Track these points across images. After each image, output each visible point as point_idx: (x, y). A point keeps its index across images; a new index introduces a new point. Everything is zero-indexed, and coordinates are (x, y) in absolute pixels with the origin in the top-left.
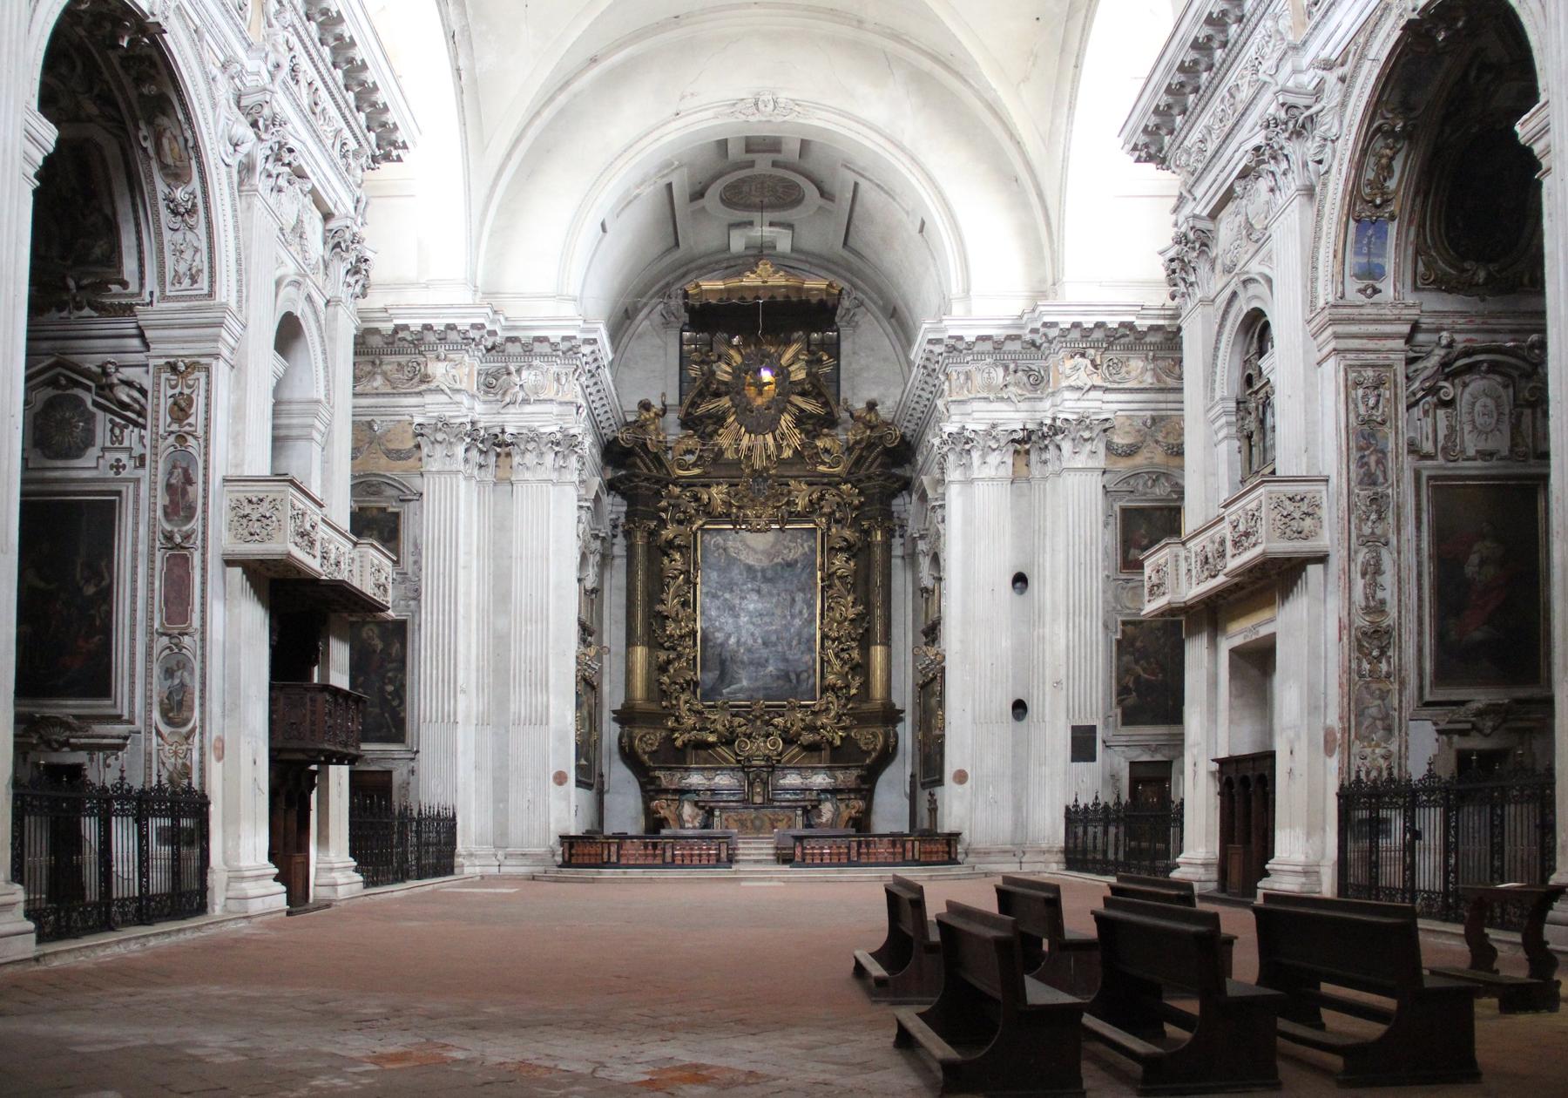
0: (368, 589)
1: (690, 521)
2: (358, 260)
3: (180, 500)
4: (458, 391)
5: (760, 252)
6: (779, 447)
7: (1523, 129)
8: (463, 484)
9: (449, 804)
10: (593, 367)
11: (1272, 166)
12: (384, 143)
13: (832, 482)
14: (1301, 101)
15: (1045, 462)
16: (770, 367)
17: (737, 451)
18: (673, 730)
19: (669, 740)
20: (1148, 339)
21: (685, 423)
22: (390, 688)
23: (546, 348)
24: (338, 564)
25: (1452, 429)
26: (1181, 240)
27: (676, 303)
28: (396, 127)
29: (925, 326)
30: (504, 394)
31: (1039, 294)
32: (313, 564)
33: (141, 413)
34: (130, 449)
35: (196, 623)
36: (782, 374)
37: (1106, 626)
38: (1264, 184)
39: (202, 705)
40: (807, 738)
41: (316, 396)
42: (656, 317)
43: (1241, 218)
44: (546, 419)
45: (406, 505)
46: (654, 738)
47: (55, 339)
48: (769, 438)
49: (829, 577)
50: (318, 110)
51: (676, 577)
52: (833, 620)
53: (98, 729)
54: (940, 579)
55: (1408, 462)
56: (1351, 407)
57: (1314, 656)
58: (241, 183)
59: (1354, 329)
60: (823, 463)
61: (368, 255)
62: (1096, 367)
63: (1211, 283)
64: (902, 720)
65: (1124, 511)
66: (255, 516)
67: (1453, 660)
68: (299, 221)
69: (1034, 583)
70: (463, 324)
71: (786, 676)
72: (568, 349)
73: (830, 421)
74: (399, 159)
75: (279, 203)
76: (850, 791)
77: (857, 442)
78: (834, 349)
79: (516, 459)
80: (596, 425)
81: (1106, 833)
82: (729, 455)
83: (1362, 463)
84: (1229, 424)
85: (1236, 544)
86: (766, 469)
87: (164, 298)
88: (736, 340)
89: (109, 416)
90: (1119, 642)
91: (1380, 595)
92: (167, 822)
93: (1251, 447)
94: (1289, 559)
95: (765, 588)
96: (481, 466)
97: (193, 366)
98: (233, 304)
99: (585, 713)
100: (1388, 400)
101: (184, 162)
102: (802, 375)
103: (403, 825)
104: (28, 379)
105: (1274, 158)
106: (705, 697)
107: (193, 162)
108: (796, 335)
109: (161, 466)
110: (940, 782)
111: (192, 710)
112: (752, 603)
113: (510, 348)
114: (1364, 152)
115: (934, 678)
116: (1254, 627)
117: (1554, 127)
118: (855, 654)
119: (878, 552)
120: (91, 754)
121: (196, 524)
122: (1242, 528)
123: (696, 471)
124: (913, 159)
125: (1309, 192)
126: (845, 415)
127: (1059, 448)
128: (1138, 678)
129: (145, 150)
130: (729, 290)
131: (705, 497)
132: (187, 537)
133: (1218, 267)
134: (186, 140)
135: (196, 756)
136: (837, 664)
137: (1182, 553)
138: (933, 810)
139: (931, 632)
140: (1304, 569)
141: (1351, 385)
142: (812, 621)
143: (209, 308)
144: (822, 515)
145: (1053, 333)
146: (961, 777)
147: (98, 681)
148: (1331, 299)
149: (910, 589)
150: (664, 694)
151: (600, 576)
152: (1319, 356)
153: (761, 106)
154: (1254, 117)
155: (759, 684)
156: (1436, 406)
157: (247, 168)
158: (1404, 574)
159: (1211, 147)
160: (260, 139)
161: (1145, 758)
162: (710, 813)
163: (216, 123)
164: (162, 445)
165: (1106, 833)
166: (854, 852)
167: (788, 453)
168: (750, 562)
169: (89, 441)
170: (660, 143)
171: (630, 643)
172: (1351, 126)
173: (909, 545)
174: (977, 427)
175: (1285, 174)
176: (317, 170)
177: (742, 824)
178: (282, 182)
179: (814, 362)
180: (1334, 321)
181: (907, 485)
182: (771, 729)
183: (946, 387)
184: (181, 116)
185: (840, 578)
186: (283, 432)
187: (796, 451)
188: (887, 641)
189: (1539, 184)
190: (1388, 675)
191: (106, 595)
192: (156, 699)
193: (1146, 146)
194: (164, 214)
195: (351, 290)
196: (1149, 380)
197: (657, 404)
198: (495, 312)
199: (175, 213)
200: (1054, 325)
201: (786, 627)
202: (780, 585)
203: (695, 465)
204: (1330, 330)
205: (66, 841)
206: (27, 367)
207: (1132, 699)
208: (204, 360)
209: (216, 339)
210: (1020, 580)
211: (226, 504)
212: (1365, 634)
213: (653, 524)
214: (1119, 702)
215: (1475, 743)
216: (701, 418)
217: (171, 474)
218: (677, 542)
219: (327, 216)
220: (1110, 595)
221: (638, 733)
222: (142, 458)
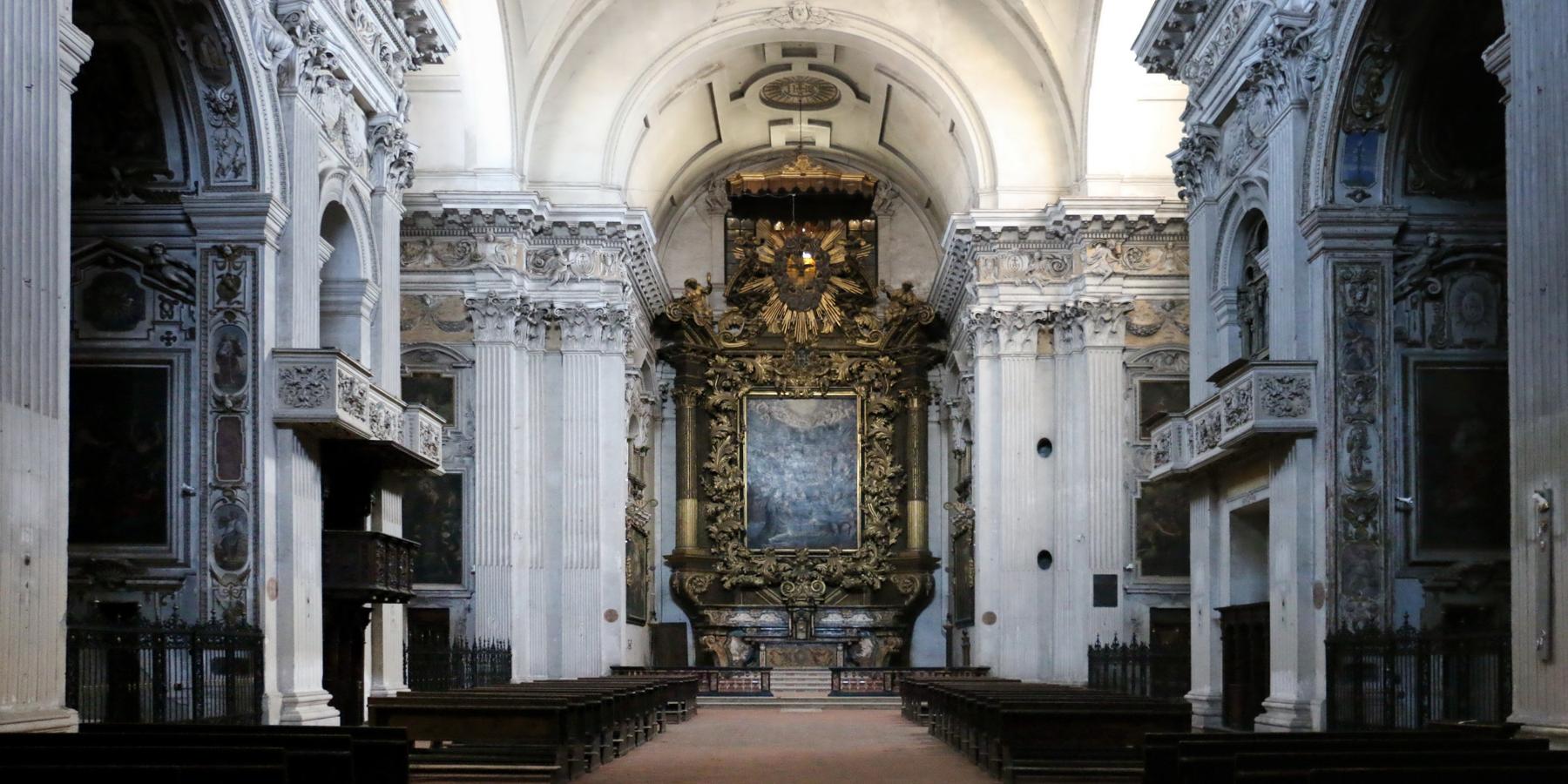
0: (420, 450)
1: (736, 387)
2: (402, 154)
3: (232, 366)
4: (508, 270)
5: (799, 149)
6: (820, 323)
7: (1489, 58)
8: (514, 353)
9: (504, 638)
10: (639, 249)
11: (1269, 81)
12: (423, 47)
13: (872, 355)
14: (1297, 23)
15: (1068, 341)
16: (811, 251)
17: (780, 326)
18: (722, 574)
19: (718, 582)
20: (1168, 230)
21: (730, 300)
22: (447, 535)
23: (592, 232)
24: (387, 426)
25: (1440, 321)
26: (1186, 144)
27: (720, 192)
28: (434, 33)
29: (954, 217)
30: (553, 273)
31: (1066, 190)
32: (361, 426)
33: (191, 290)
34: (179, 323)
35: (248, 477)
36: (822, 257)
37: (1126, 487)
38: (1263, 97)
39: (256, 550)
40: (850, 581)
41: (363, 276)
42: (701, 204)
43: (1243, 127)
44: (593, 296)
45: (459, 372)
46: (706, 579)
47: (100, 222)
48: (811, 315)
49: (869, 441)
50: (356, 17)
51: (723, 438)
52: (872, 477)
53: (154, 571)
54: (970, 443)
55: (1395, 350)
56: (1339, 299)
57: (1304, 520)
58: (280, 85)
59: (1343, 230)
60: (862, 337)
61: (412, 148)
62: (1117, 255)
63: (1216, 185)
64: (938, 567)
65: (1144, 385)
66: (304, 386)
67: (1438, 524)
68: (341, 119)
69: (1058, 448)
70: (511, 209)
71: (828, 527)
72: (614, 233)
73: (868, 300)
74: (439, 61)
75: (320, 103)
76: (888, 629)
77: (894, 320)
78: (872, 236)
79: (565, 332)
80: (644, 302)
81: (1124, 669)
82: (773, 329)
83: (1349, 349)
84: (1230, 311)
85: (1229, 419)
86: (808, 342)
87: (208, 188)
88: (778, 226)
89: (159, 293)
90: (1139, 502)
91: (1366, 466)
92: (222, 654)
93: (1251, 333)
94: (1278, 434)
95: (808, 448)
96: (531, 338)
97: (240, 250)
98: (277, 194)
99: (637, 558)
100: (1376, 294)
101: (223, 62)
102: (841, 259)
103: (458, 657)
104: (73, 259)
105: (1272, 74)
106: (752, 544)
107: (232, 66)
108: (834, 223)
109: (210, 338)
110: (972, 623)
111: (245, 554)
112: (798, 460)
113: (557, 231)
114: (1354, 71)
115: (965, 531)
116: (1251, 493)
117: (1515, 59)
118: (894, 508)
119: (915, 417)
120: (147, 594)
121: (247, 390)
122: (1234, 405)
123: (742, 344)
124: (942, 65)
125: (1302, 105)
126: (882, 296)
127: (1081, 328)
128: (1158, 536)
129: (183, 53)
130: (768, 181)
131: (750, 367)
132: (238, 402)
133: (1223, 172)
134: (224, 46)
135: (250, 595)
136: (877, 517)
137: (1185, 426)
138: (966, 648)
139: (964, 489)
140: (1293, 443)
141: (1338, 281)
142: (853, 478)
143: (253, 198)
144: (862, 384)
145: (1075, 225)
146: (990, 618)
147: (154, 528)
148: (1321, 203)
149: (945, 451)
150: (713, 542)
151: (651, 436)
152: (1310, 254)
153: (796, 14)
154: (1254, 36)
155: (803, 533)
156: (1424, 300)
157: (286, 71)
158: (1390, 449)
159: (1217, 61)
160: (297, 44)
161: (1166, 605)
162: (756, 648)
163: (253, 31)
164: (211, 321)
165: (1124, 669)
166: (889, 683)
167: (828, 329)
168: (794, 424)
169: (138, 316)
170: (697, 48)
171: (680, 495)
172: (1341, 47)
173: (945, 412)
174: (1003, 309)
175: (1280, 88)
176: (357, 71)
177: (786, 657)
178: (323, 84)
179: (852, 246)
180: (1322, 223)
181: (942, 358)
182: (815, 574)
183: (974, 272)
184: (218, 24)
185: (879, 440)
186: (332, 308)
187: (836, 326)
188: (924, 496)
189: (1502, 108)
190: (1374, 538)
191: (160, 453)
192: (210, 545)
193: (1157, 59)
194: (206, 112)
195: (395, 181)
196: (1168, 268)
197: (702, 283)
198: (542, 199)
199: (217, 111)
200: (1076, 217)
201: (829, 484)
202: (823, 446)
203: (740, 338)
204: (1319, 231)
205: (122, 669)
206: (73, 248)
207: (1152, 552)
208: (250, 245)
209: (262, 226)
210: (1045, 446)
211: (275, 373)
212: (1351, 501)
213: (700, 391)
214: (1139, 555)
215: (1463, 599)
216: (745, 296)
217: (220, 346)
218: (724, 406)
219: (369, 114)
220: (1130, 460)
221: (688, 576)
222: (192, 332)
